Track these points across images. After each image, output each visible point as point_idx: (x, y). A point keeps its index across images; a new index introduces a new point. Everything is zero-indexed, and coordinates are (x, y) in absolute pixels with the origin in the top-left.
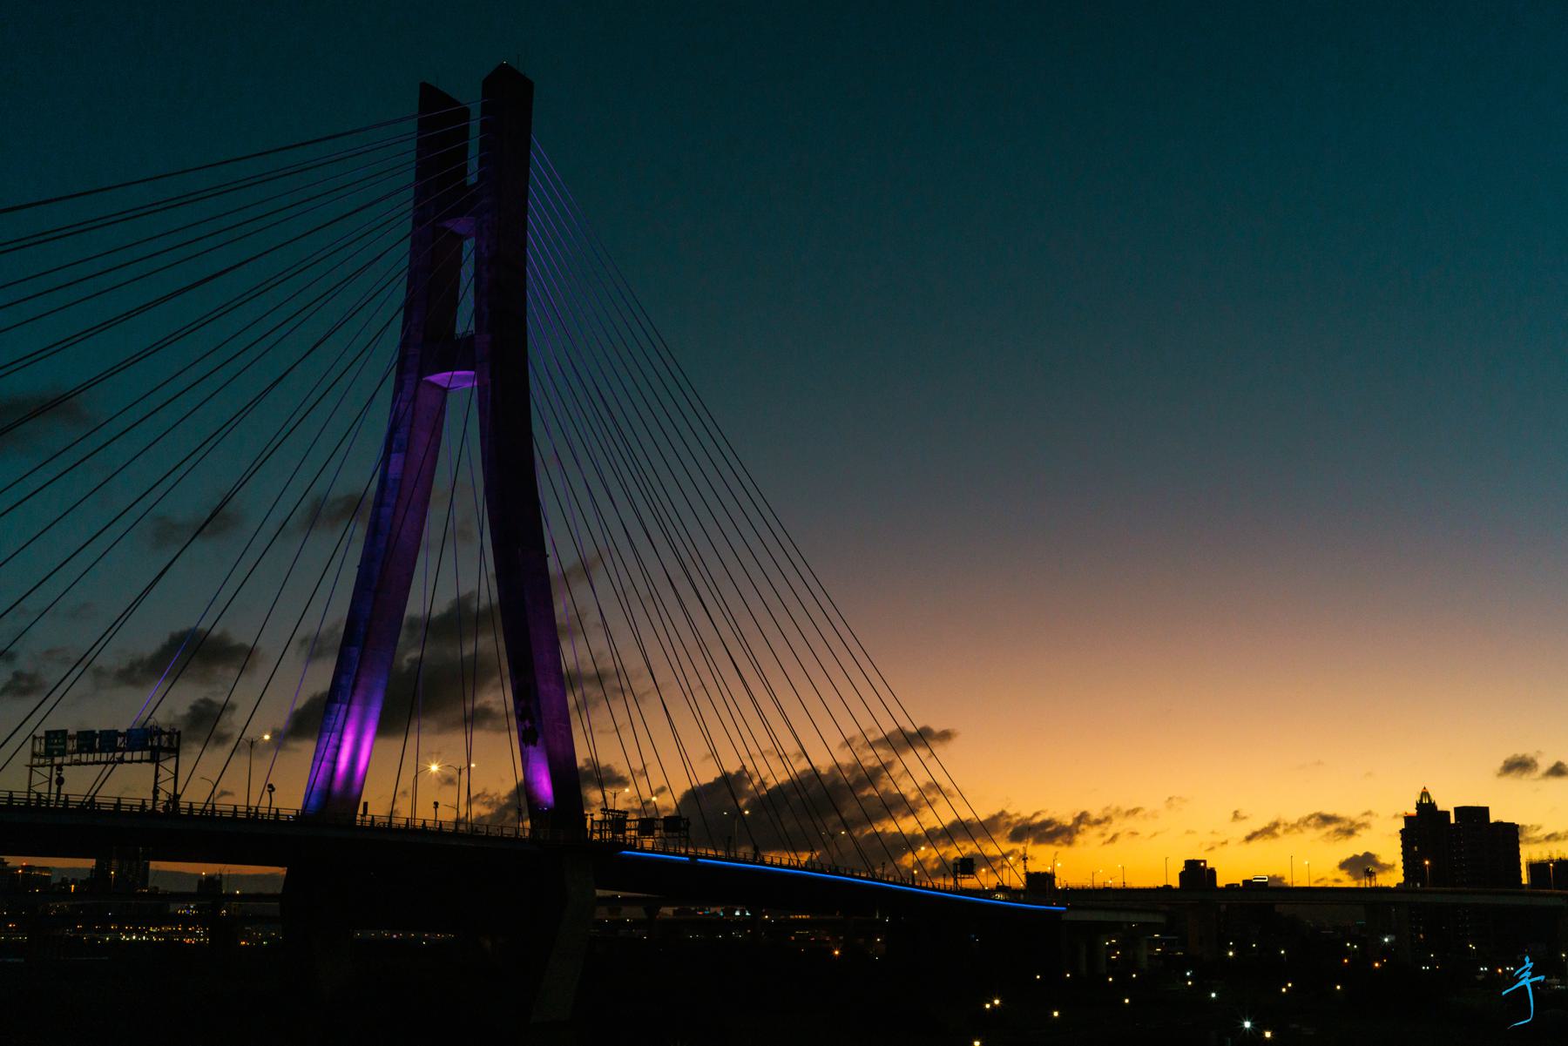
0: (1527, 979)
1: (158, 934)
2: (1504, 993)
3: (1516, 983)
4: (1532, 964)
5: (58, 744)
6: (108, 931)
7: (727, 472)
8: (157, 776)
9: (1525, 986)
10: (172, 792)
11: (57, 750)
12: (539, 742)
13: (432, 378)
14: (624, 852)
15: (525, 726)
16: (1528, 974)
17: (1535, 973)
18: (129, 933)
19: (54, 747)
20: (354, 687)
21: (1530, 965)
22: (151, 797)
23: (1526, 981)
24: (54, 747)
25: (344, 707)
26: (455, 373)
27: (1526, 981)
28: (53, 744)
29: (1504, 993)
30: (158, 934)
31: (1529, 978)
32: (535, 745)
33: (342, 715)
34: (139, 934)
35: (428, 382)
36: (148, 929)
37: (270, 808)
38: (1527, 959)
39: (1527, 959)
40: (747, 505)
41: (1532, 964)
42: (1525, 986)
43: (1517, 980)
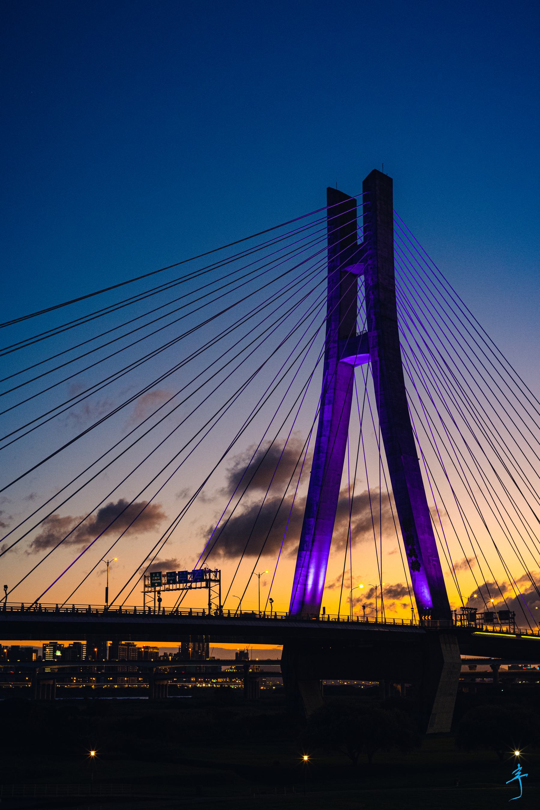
0: (519, 776)
2: (507, 783)
3: (513, 778)
4: (521, 768)
5: (157, 580)
6: (190, 682)
8: (210, 596)
9: (518, 779)
10: (218, 604)
11: (157, 583)
13: (345, 360)
14: (476, 633)
15: (412, 560)
16: (519, 773)
17: (523, 772)
18: (201, 682)
19: (156, 581)
20: (313, 541)
23: (518, 777)
24: (156, 581)
25: (308, 553)
27: (518, 777)
28: (155, 580)
29: (507, 783)
31: (520, 775)
32: (419, 571)
33: (307, 557)
34: (207, 682)
35: (343, 362)
36: (211, 680)
38: (519, 765)
39: (519, 765)
41: (521, 768)
42: (518, 779)
43: (514, 776)
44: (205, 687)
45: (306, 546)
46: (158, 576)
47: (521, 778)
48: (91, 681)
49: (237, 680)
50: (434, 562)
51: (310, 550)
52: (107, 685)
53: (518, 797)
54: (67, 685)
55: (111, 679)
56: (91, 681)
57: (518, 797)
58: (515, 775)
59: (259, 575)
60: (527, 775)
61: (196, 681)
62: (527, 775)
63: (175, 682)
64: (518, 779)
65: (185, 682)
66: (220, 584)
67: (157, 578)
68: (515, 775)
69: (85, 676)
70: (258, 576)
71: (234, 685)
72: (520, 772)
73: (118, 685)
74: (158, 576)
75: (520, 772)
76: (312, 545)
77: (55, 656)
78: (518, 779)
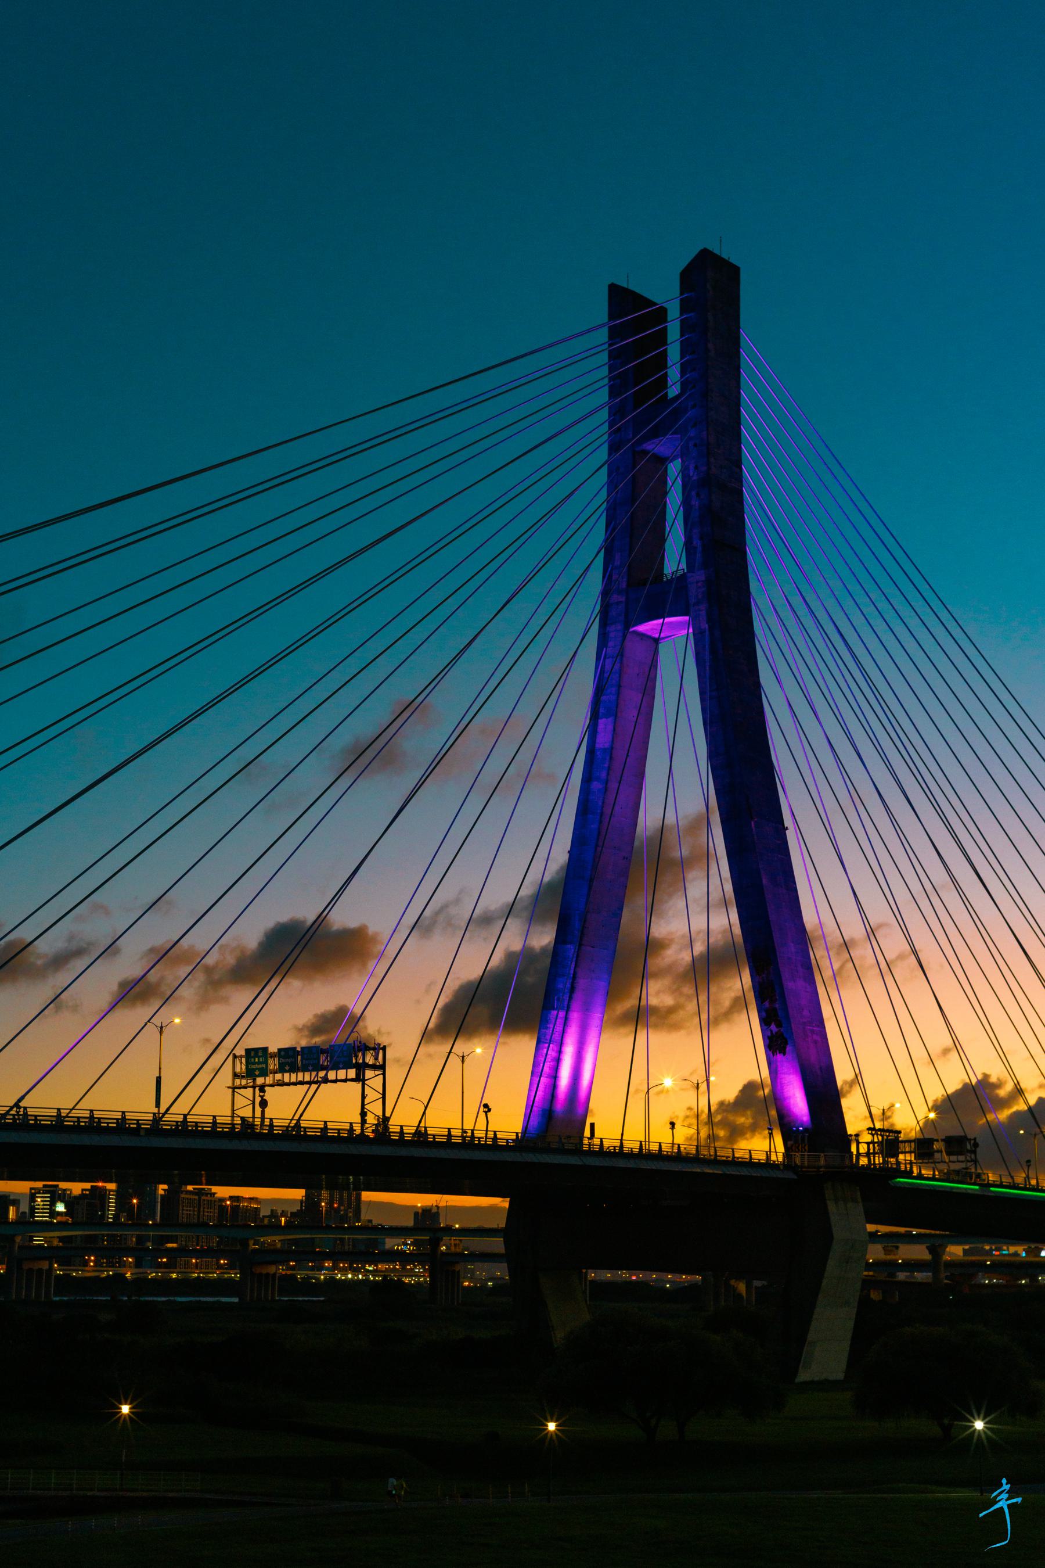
0: (1004, 1501)
1: (374, 1273)
2: (981, 1515)
3: (993, 1506)
4: (1009, 1485)
5: (259, 1063)
7: (967, 757)
8: (363, 1097)
9: (1002, 1508)
10: (380, 1114)
11: (259, 1069)
12: (789, 1048)
13: (642, 628)
14: (898, 1180)
15: (771, 1031)
16: (1005, 1496)
17: (1012, 1494)
18: (344, 1271)
20: (572, 989)
21: (1006, 1487)
22: (359, 1120)
25: (562, 1014)
26: (667, 620)
29: (981, 1515)
30: (374, 1273)
31: (1006, 1500)
33: (560, 1022)
35: (635, 632)
37: (487, 1131)
38: (1004, 1481)
39: (1004, 1481)
40: (967, 757)
41: (1009, 1485)
42: (1002, 1508)
43: (995, 1502)
44: (352, 1280)
45: (558, 999)
46: (261, 1056)
47: (1009, 1506)
48: (123, 1265)
49: (415, 1266)
50: (815, 1036)
51: (566, 1009)
52: (157, 1273)
53: (1003, 1543)
54: (76, 1271)
55: (165, 1260)
56: (123, 1265)
57: (1003, 1543)
58: (997, 1499)
59: (463, 1057)
60: (1019, 1500)
61: (335, 1267)
62: (1019, 1500)
63: (293, 1268)
64: (1002, 1507)
65: (312, 1269)
66: (384, 1074)
67: (259, 1060)
68: (997, 1499)
69: (112, 1253)
70: (461, 1058)
71: (411, 1276)
72: (1007, 1495)
73: (178, 1273)
74: (261, 1056)
75: (1007, 1495)
76: (570, 998)
77: (53, 1213)
78: (1002, 1507)
